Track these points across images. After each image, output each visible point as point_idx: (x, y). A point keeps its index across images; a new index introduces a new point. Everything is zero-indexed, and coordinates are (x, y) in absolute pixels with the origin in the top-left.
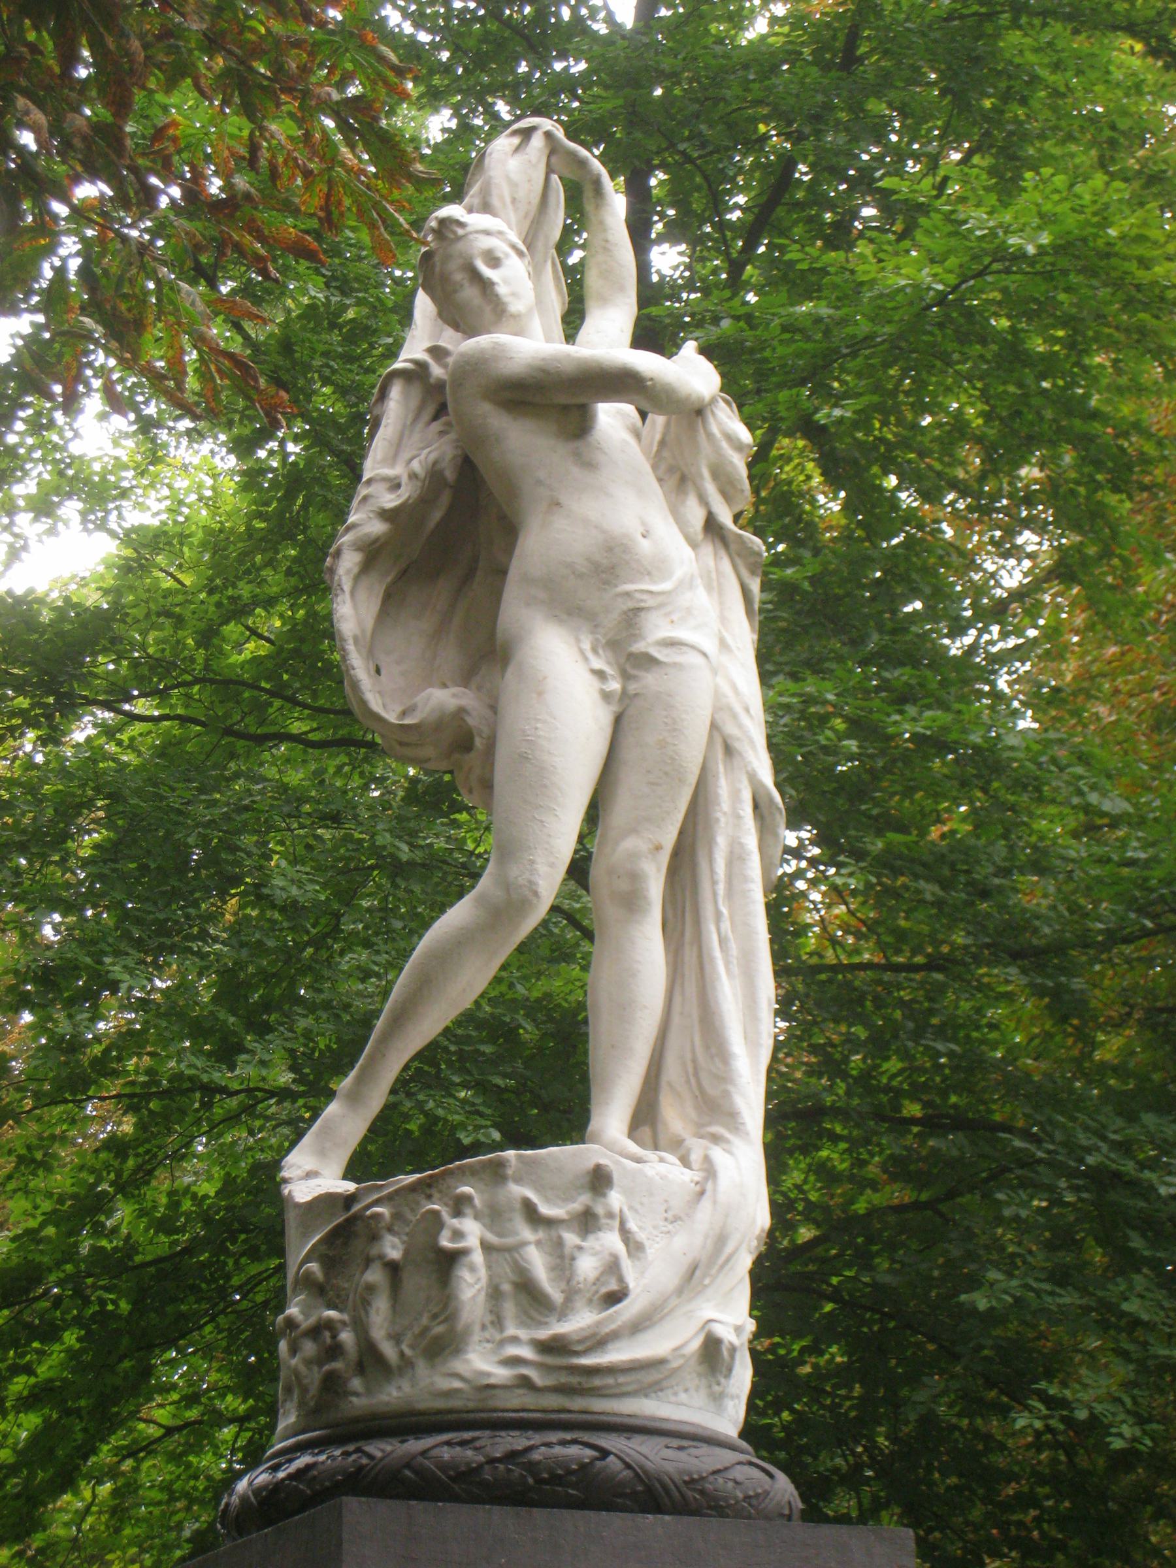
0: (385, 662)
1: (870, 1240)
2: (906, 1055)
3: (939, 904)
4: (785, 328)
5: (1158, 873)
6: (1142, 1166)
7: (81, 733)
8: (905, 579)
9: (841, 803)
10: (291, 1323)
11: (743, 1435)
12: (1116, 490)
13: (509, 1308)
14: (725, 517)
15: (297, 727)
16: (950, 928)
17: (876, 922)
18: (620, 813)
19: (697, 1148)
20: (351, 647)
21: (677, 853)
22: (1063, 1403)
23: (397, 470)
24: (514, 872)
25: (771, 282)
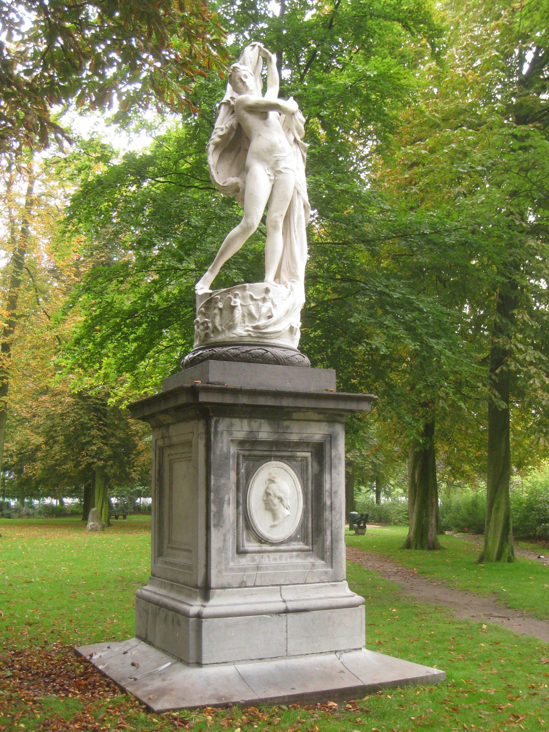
0: (219, 171)
1: (328, 306)
2: (337, 264)
3: (346, 229)
4: (314, 92)
5: (397, 223)
6: (390, 291)
7: (145, 184)
8: (340, 153)
9: (324, 205)
10: (197, 322)
11: (298, 348)
12: (390, 133)
13: (246, 319)
14: (299, 139)
15: (196, 184)
16: (348, 235)
17: (331, 233)
18: (273, 207)
19: (289, 284)
20: (212, 168)
21: (286, 217)
22: (370, 344)
23: (223, 126)
24: (249, 220)
25: (311, 80)
